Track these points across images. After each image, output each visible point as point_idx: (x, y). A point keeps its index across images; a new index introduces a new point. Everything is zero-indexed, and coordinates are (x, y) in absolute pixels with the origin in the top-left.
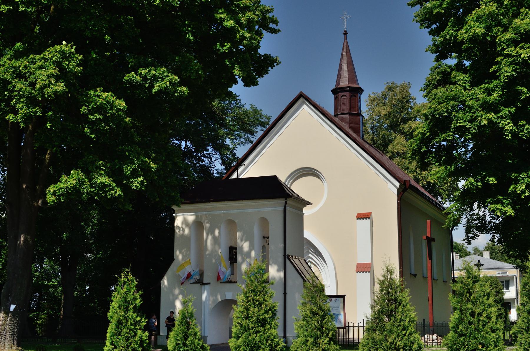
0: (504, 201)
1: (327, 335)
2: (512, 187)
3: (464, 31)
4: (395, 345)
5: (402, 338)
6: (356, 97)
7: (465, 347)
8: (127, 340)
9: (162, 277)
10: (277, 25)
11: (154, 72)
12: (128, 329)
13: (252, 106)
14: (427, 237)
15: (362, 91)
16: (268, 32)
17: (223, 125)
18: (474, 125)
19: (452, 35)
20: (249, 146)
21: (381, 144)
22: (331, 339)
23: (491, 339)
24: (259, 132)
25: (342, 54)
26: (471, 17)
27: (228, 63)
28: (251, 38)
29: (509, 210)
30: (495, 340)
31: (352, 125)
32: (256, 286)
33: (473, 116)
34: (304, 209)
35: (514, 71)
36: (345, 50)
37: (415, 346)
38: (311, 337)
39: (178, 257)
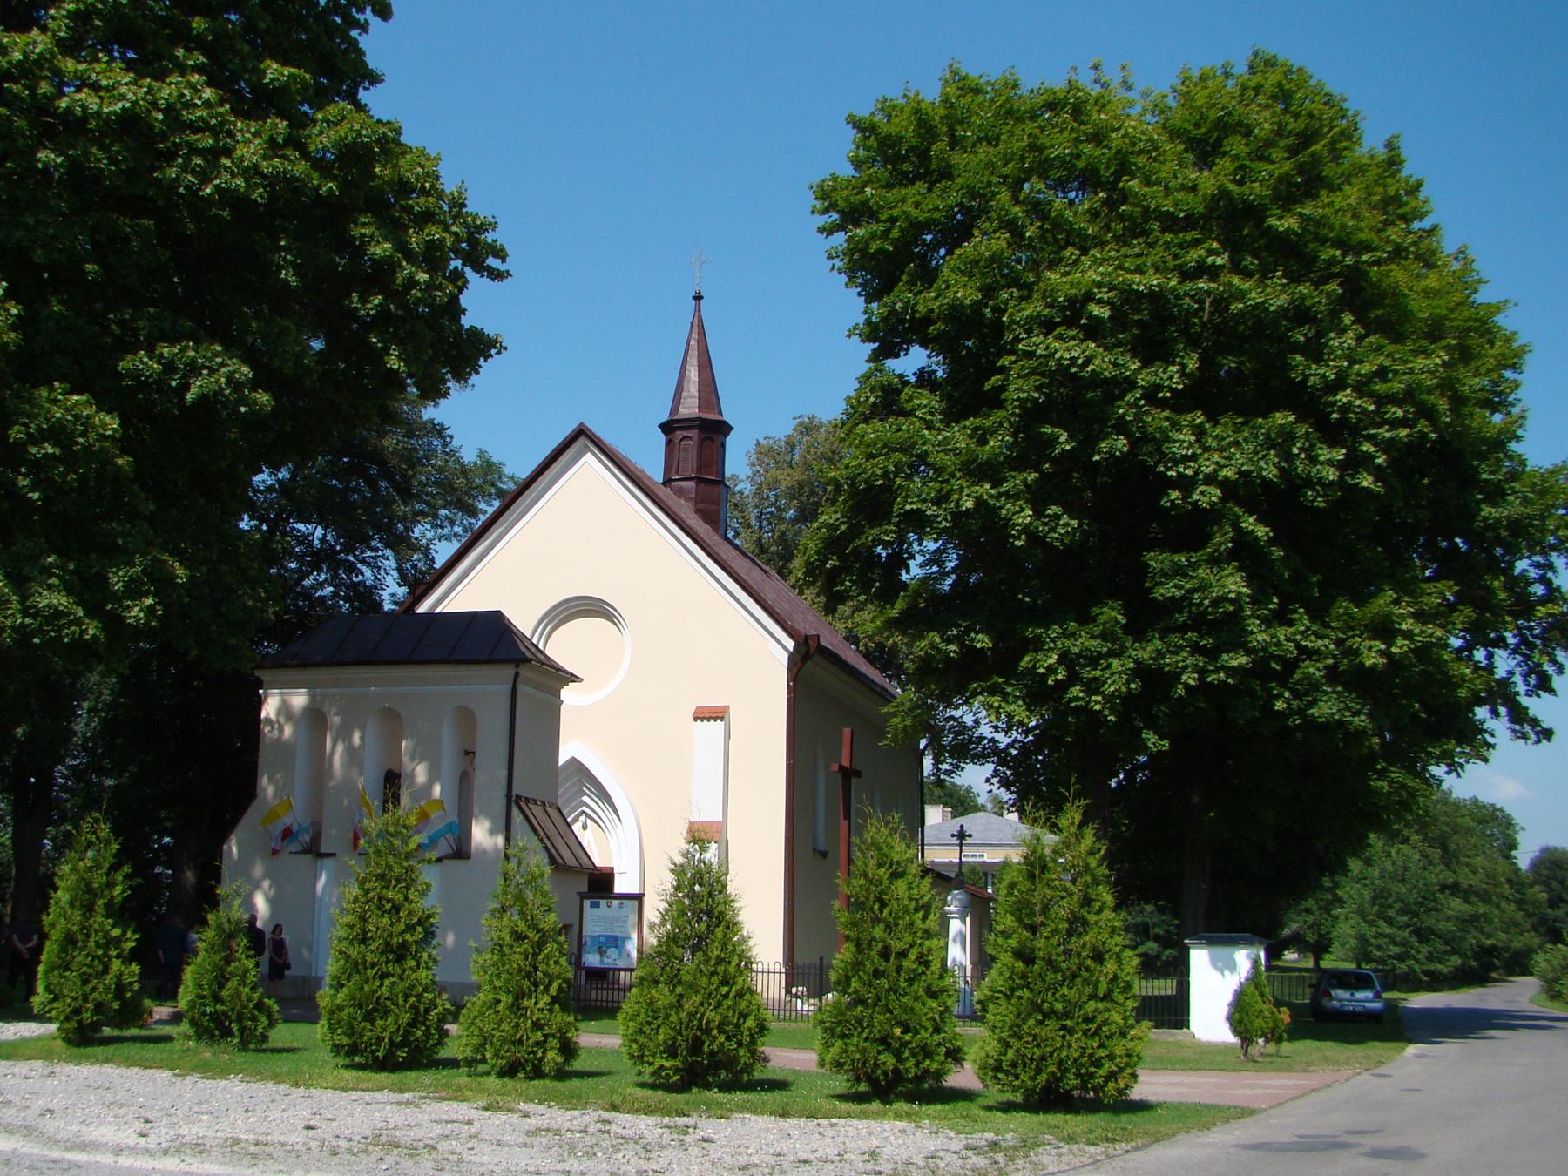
0: (1009, 690)
1: (547, 989)
2: (1027, 659)
3: (933, 294)
4: (701, 1019)
5: (719, 1005)
6: (713, 440)
7: (863, 1031)
8: (85, 982)
9: (224, 837)
10: (503, 260)
11: (192, 353)
12: (88, 955)
13: (481, 453)
14: (841, 767)
15: (730, 428)
16: (482, 276)
17: (406, 494)
18: (945, 510)
19: (908, 302)
20: (455, 546)
21: (777, 553)
22: (554, 1000)
23: (925, 1014)
24: (488, 508)
25: (688, 344)
26: (952, 262)
27: (374, 340)
28: (430, 286)
29: (1018, 710)
30: (937, 1016)
31: (701, 506)
32: (388, 866)
33: (942, 489)
34: (562, 691)
35: (1038, 389)
36: (695, 335)
37: (750, 1022)
38: (509, 992)
39: (265, 790)
